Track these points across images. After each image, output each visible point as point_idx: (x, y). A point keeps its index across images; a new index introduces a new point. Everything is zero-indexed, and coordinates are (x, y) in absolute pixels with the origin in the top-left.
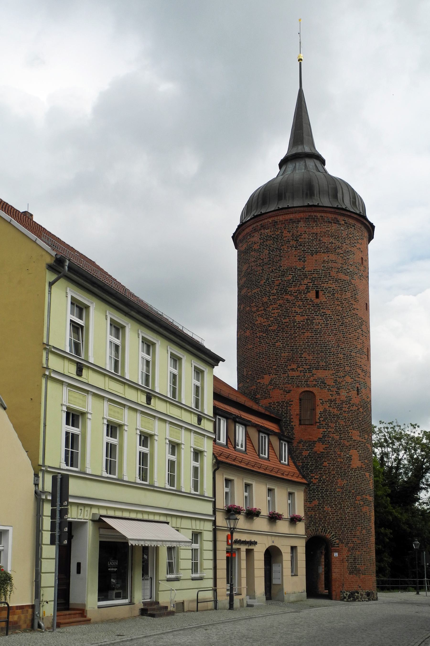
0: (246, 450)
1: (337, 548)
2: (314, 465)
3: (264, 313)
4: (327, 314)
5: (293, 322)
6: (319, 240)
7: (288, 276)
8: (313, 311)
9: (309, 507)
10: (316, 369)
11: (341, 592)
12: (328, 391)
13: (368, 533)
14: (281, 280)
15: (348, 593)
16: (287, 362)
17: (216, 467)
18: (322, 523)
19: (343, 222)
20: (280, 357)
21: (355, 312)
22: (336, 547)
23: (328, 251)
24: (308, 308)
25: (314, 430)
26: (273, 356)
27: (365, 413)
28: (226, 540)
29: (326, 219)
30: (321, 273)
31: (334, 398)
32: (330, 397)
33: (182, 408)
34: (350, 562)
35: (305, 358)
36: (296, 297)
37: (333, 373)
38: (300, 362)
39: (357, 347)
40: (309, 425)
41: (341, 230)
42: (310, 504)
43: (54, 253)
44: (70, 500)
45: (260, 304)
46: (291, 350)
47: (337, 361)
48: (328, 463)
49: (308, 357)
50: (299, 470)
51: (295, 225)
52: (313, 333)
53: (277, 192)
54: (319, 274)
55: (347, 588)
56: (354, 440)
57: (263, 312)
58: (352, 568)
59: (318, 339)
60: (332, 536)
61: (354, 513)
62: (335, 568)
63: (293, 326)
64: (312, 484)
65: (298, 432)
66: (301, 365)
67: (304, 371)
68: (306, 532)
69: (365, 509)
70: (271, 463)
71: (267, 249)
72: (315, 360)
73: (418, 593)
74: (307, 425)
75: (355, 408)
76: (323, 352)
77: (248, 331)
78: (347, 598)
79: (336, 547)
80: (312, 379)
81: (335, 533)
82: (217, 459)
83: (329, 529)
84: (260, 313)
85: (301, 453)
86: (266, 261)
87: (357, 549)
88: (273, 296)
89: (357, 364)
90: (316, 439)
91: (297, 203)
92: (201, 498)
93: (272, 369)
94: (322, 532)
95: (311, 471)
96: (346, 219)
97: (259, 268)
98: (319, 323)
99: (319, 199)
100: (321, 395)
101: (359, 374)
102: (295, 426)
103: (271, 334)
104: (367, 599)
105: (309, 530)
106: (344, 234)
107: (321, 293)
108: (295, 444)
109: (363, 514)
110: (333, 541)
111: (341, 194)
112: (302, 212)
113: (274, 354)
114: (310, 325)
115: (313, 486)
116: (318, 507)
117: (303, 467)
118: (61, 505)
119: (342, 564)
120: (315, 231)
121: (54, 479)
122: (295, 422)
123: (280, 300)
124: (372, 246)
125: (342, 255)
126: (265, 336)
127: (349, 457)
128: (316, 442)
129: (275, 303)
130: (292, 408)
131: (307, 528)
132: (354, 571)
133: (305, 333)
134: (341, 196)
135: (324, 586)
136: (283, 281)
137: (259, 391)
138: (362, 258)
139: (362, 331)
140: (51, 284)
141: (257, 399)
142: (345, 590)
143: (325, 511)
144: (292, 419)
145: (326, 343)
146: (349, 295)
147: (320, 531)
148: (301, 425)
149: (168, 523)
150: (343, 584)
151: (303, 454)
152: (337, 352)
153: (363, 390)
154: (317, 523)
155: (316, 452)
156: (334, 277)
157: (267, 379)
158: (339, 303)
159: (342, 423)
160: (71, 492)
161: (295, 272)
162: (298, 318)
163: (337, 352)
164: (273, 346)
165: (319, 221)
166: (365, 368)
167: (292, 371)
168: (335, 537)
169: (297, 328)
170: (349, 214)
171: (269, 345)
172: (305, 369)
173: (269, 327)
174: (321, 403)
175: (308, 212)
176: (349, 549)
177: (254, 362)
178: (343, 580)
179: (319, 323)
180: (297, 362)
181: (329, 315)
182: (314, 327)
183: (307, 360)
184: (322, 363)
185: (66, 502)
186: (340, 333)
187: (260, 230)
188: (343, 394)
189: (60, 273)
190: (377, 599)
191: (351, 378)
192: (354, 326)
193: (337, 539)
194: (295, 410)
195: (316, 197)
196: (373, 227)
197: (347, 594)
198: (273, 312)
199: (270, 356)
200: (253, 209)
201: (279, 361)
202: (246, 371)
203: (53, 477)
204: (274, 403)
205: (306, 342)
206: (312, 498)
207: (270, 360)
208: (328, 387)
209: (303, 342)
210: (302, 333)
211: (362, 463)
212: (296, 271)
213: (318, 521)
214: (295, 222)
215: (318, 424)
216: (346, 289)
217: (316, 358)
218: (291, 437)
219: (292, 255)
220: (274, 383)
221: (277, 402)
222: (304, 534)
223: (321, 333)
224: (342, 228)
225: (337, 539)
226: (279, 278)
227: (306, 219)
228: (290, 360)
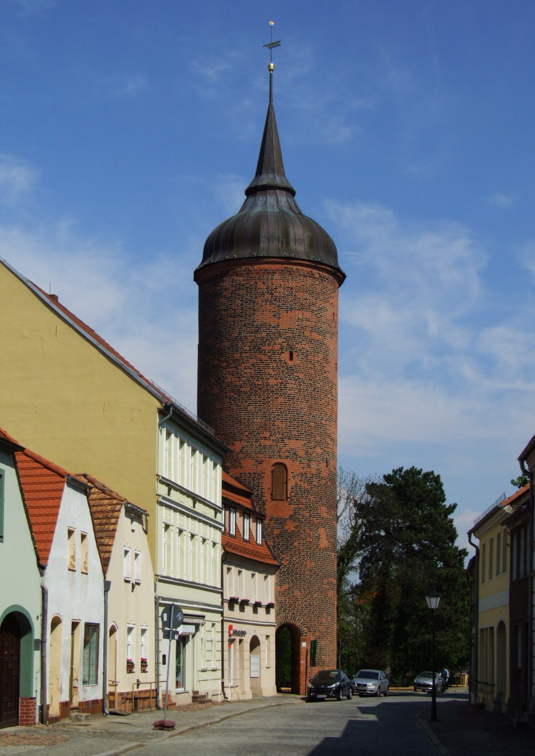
6: (295, 296)
14: (255, 336)
23: (302, 308)
25: (285, 506)
29: (302, 272)
49: (280, 425)
65: (270, 508)
68: (276, 619)
71: (239, 299)
75: (324, 482)
80: (284, 449)
81: (304, 620)
82: (225, 550)
84: (230, 370)
90: (287, 517)
98: (293, 388)
100: (293, 467)
106: (319, 288)
107: (295, 355)
117: (274, 547)
122: (267, 497)
125: (315, 313)
130: (264, 481)
131: (277, 615)
146: (321, 356)
147: (290, 618)
153: (331, 462)
155: (287, 531)
172: (277, 438)
173: (241, 387)
179: (293, 388)
184: (294, 433)
188: (312, 466)
194: (267, 483)
204: (245, 473)
214: (270, 273)
218: (262, 513)
222: (274, 621)
224: (317, 282)
226: (252, 333)
227: (282, 271)
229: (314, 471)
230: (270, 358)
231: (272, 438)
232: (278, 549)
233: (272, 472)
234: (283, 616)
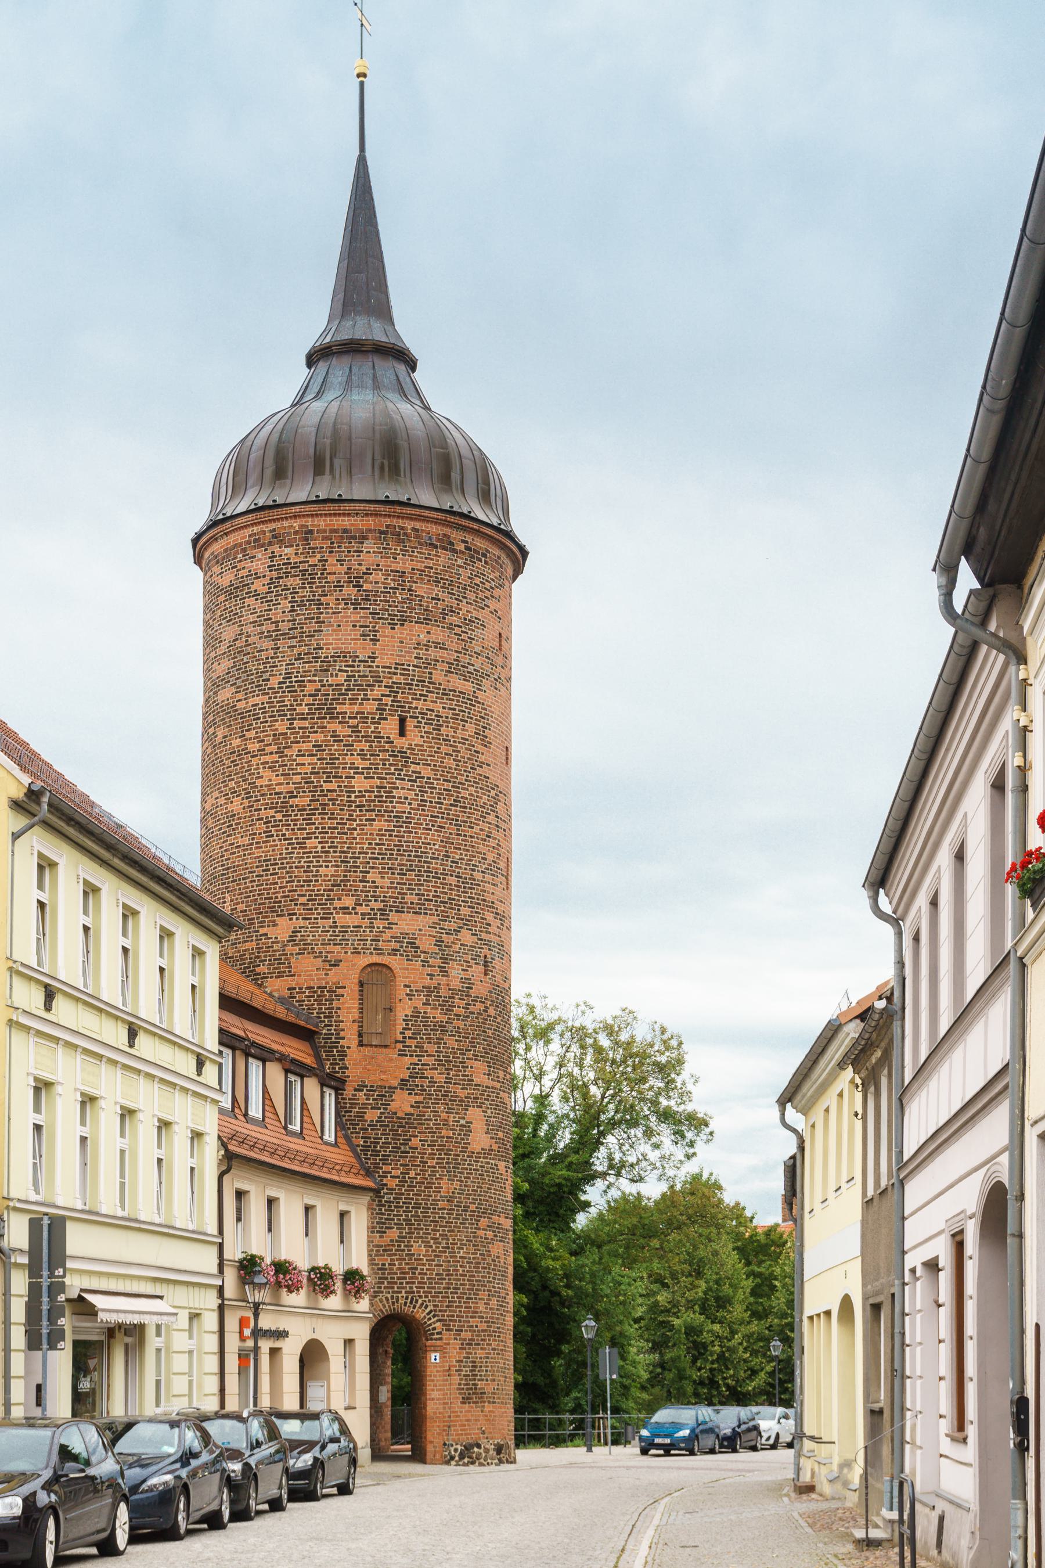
0: (263, 1120)
1: (438, 1343)
2: (390, 1143)
3: (277, 762)
5: (347, 792)
7: (337, 675)
8: (393, 768)
9: (378, 1246)
10: (397, 911)
11: (445, 1444)
13: (501, 1306)
15: (459, 1448)
16: (332, 890)
17: (224, 1168)
18: (407, 1283)
20: (316, 876)
21: (484, 771)
22: (436, 1339)
24: (381, 760)
25: (391, 1060)
26: (299, 872)
27: (499, 1019)
28: (238, 1330)
31: (435, 982)
32: (427, 981)
33: (175, 1043)
35: (374, 882)
36: (355, 731)
38: (362, 891)
39: (486, 859)
40: (381, 1046)
41: (458, 566)
42: (381, 1237)
43: (26, 780)
44: (69, 1264)
45: (269, 735)
46: (342, 862)
49: (379, 882)
50: (357, 1156)
51: (355, 545)
52: (392, 821)
53: (312, 451)
54: (408, 675)
55: (457, 1435)
57: (276, 757)
58: (468, 1389)
59: (403, 837)
60: (428, 1314)
61: (474, 1258)
62: (433, 1390)
63: (348, 801)
65: (357, 1064)
66: (364, 901)
69: (497, 1248)
70: (308, 1144)
71: (286, 598)
73: (590, 1450)
74: (376, 1046)
75: (479, 1006)
76: (414, 870)
77: (236, 801)
78: (457, 1458)
79: (436, 1339)
80: (388, 934)
81: (434, 1306)
82: (227, 1150)
83: (420, 1297)
84: (267, 758)
85: (361, 1116)
86: (284, 627)
87: (479, 1344)
88: (300, 719)
89: (485, 900)
90: (395, 1083)
91: (361, 490)
92: (194, 1237)
93: (296, 905)
94: (405, 1304)
95: (385, 1160)
96: (469, 538)
97: (267, 644)
98: (406, 798)
99: (408, 481)
100: (408, 974)
103: (296, 815)
105: (377, 1299)
107: (410, 724)
108: (349, 1092)
109: (493, 1261)
110: (430, 1325)
111: (458, 471)
112: (371, 515)
113: (303, 867)
114: (386, 802)
116: (399, 1246)
118: (51, 1275)
119: (447, 1380)
120: (399, 567)
121: (35, 1225)
122: (350, 1039)
123: (316, 732)
124: (518, 587)
125: (457, 630)
126: (281, 821)
128: (396, 1088)
129: (305, 739)
132: (472, 1395)
133: (374, 820)
134: (458, 477)
135: (389, 1435)
136: (324, 686)
137: (265, 956)
138: (500, 634)
139: (497, 817)
140: (16, 836)
141: (259, 974)
142: (453, 1440)
143: (413, 1255)
146: (471, 728)
148: (362, 1046)
149: (161, 1297)
150: (449, 1427)
151: (366, 1117)
152: (444, 869)
153: (497, 963)
154: (396, 1283)
155: (396, 1113)
156: (440, 684)
157: (282, 929)
158: (450, 750)
159: (452, 1043)
160: (69, 1251)
161: (353, 666)
162: (360, 783)
163: (444, 869)
165: (410, 541)
166: (501, 908)
167: (344, 913)
168: (434, 1316)
169: (356, 806)
170: (475, 526)
171: (289, 844)
172: (372, 909)
173: (290, 797)
174: (407, 995)
175: (385, 515)
176: (462, 1344)
177: (251, 882)
178: (450, 1417)
180: (356, 891)
181: (429, 778)
183: (377, 887)
185: (61, 1270)
186: (451, 824)
187: (270, 544)
188: (453, 973)
189: (35, 816)
190: (514, 1462)
193: (438, 1321)
194: (348, 1010)
195: (402, 479)
196: (525, 554)
197: (456, 1450)
198: (299, 760)
199: (293, 872)
200: (250, 483)
201: (314, 886)
202: (232, 901)
203: (31, 1220)
204: (301, 988)
205: (376, 844)
206: (384, 1223)
207: (293, 881)
209: (370, 844)
210: (367, 820)
211: (492, 1138)
212: (357, 663)
213: (398, 1278)
214: (354, 538)
215: (400, 1046)
219: (347, 622)
220: (301, 940)
221: (307, 988)
222: (367, 1310)
223: (410, 823)
224: (460, 562)
225: (438, 1321)
226: (315, 675)
227: (381, 532)
228: (340, 885)
229: (456, 984)
234: (387, 1298)
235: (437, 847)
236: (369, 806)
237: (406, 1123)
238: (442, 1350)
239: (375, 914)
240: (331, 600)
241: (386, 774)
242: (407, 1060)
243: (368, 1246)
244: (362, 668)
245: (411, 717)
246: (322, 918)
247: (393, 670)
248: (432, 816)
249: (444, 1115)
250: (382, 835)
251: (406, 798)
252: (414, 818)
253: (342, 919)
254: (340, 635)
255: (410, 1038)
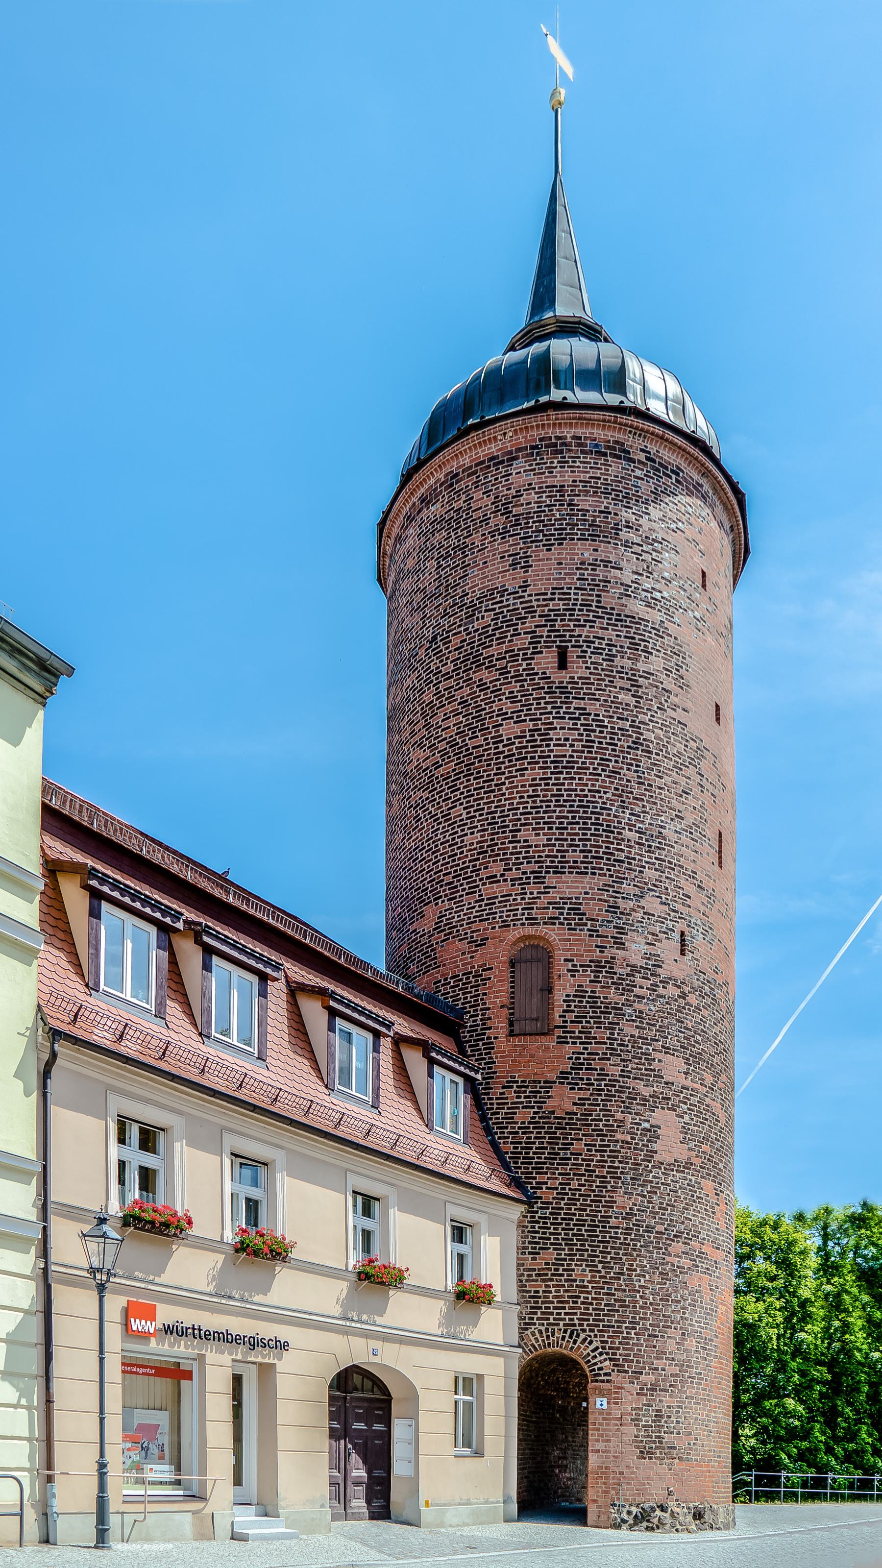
4: (590, 714)
5: (494, 743)
8: (549, 707)
10: (554, 872)
12: (591, 936)
19: (642, 457)
22: (603, 1381)
25: (547, 1048)
30: (572, 596)
34: (644, 1426)
35: (526, 841)
36: (504, 672)
37: (606, 885)
38: (512, 854)
39: (682, 818)
41: (635, 477)
47: (618, 850)
48: (586, 1145)
49: (533, 839)
54: (569, 599)
56: (666, 1083)
59: (563, 784)
60: (593, 1351)
64: (539, 1205)
67: (521, 879)
72: (554, 845)
79: (603, 1381)
80: (544, 900)
83: (584, 1331)
85: (510, 1117)
94: (563, 1338)
95: (539, 1169)
98: (567, 739)
101: (689, 897)
102: (496, 1038)
104: (694, 1527)
105: (528, 1332)
107: (572, 655)
114: (541, 746)
115: (541, 1208)
117: (515, 1156)
120: (557, 481)
122: (499, 1027)
125: (638, 549)
127: (649, 1131)
133: (526, 769)
144: (490, 1019)
145: (587, 796)
146: (656, 663)
148: (511, 1036)
155: (553, 1112)
162: (509, 730)
164: (446, 821)
165: (570, 451)
168: (601, 1354)
172: (524, 873)
174: (569, 971)
176: (642, 1389)
182: (552, 751)
183: (531, 846)
191: (661, 903)
192: (674, 755)
193: (605, 1360)
194: (497, 993)
204: (446, 979)
208: (589, 923)
210: (517, 771)
212: (504, 599)
213: (555, 1308)
216: (650, 646)
217: (556, 839)
223: (573, 768)
227: (532, 448)
230: (504, 672)
231: (509, 875)
232: (528, 1160)
233: (513, 966)
234: (540, 1332)
235: (609, 795)
236: (521, 753)
237: (567, 1122)
238: (614, 1397)
239: (529, 878)
240: (477, 538)
241: (541, 714)
242: (568, 1048)
243: (518, 1270)
244: (511, 602)
245: (573, 646)
246: (467, 894)
247: (549, 596)
248: (601, 759)
249: (619, 1116)
250: (537, 785)
251: (567, 739)
252: (577, 762)
253: (487, 890)
254: (490, 571)
255: (572, 1022)
